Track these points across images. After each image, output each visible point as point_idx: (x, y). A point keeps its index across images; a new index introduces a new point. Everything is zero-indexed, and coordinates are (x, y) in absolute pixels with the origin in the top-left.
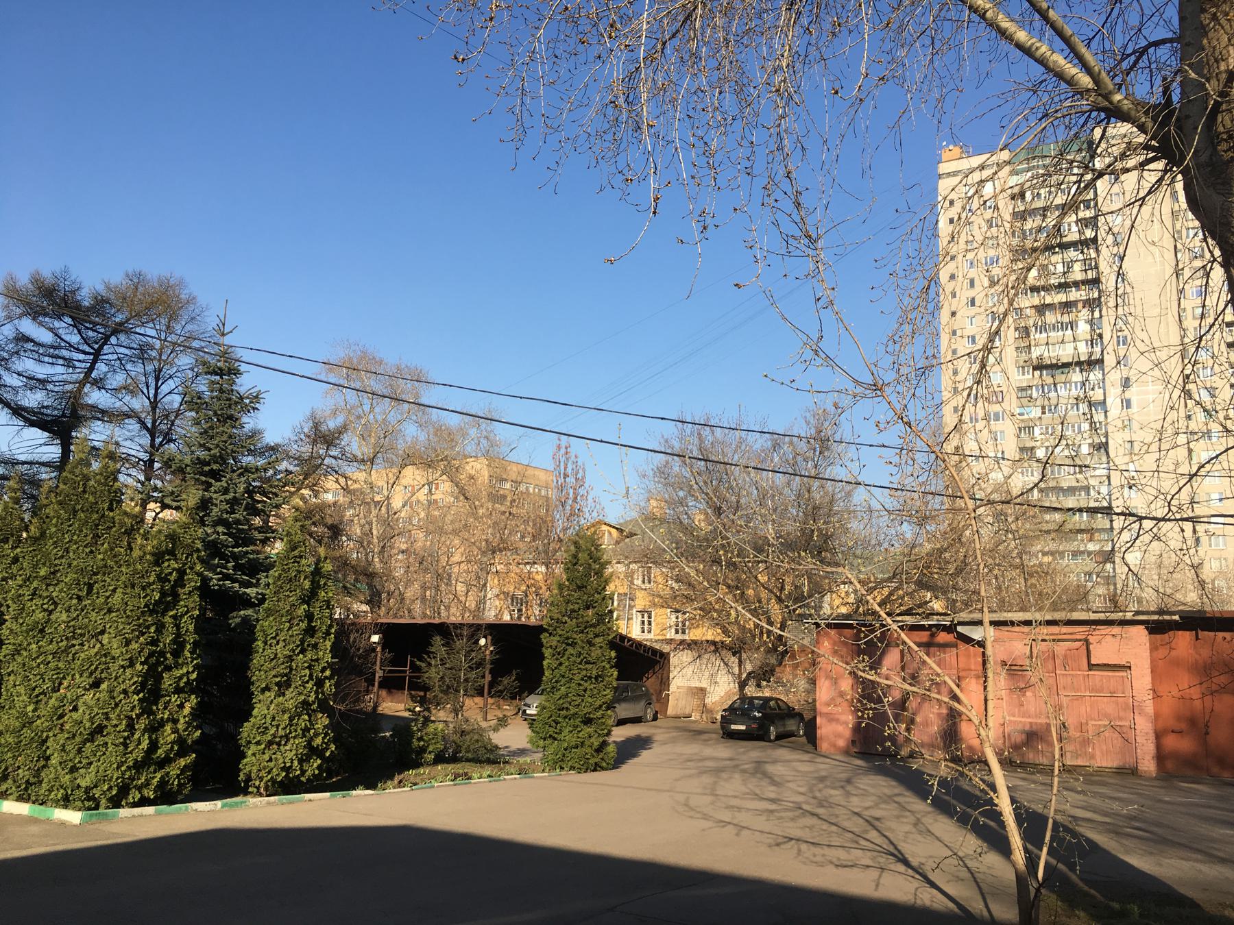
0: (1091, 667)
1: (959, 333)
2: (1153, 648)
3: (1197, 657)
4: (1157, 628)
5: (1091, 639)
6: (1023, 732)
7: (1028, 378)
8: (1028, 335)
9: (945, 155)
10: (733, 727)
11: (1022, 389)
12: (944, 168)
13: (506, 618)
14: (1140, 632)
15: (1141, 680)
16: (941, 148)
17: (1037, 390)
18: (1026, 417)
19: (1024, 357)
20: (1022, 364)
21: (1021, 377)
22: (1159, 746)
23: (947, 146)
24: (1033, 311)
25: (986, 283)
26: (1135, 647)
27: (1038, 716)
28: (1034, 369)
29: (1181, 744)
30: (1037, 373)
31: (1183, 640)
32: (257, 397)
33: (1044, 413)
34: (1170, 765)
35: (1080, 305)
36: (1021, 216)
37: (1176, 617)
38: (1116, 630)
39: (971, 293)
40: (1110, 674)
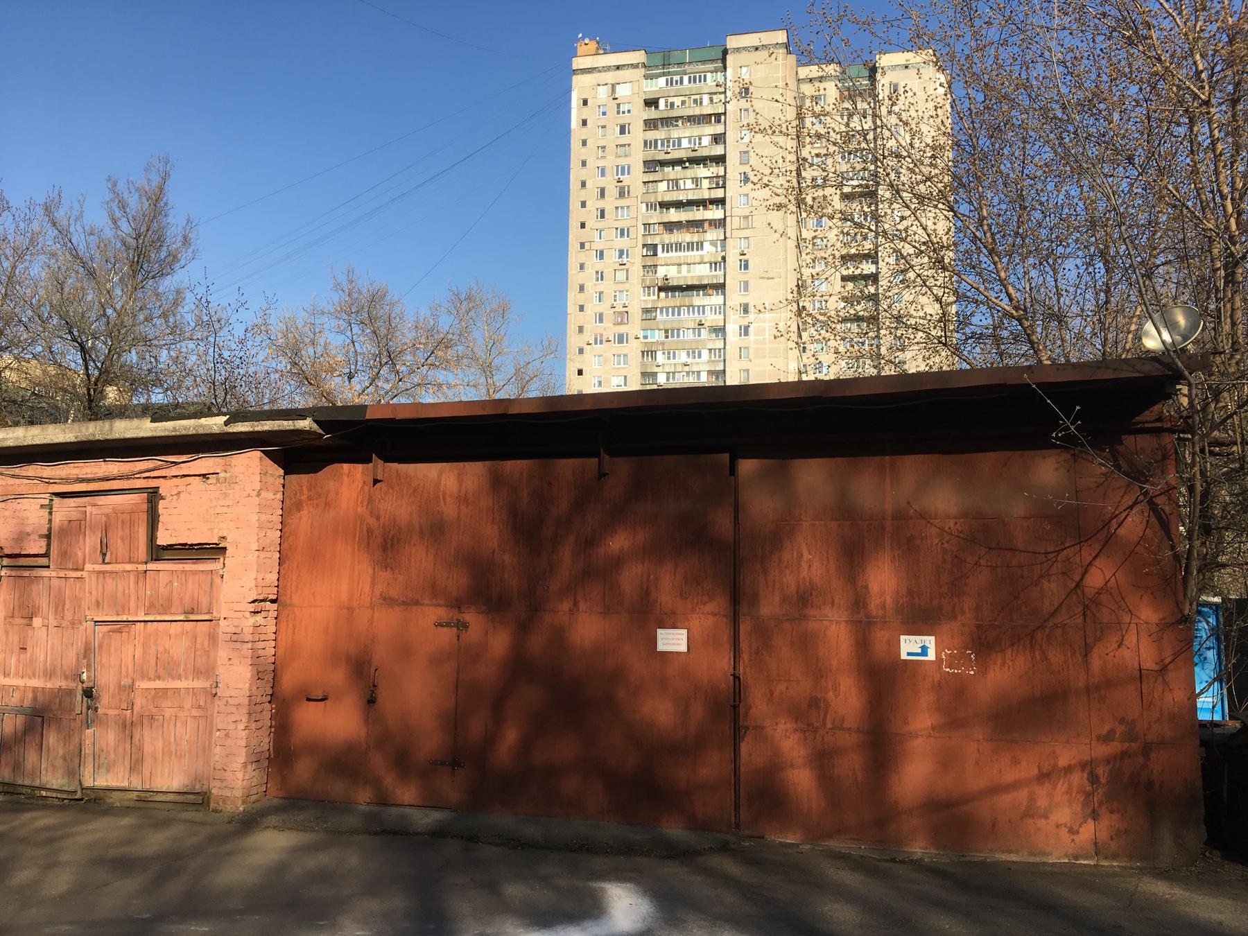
0: (157, 552)
1: (587, 246)
2: (289, 508)
3: (372, 521)
4: (295, 455)
5: (165, 487)
6: (19, 711)
7: (650, 299)
9: (581, 49)
10: (1204, 598)
12: (578, 63)
15: (243, 577)
16: (578, 40)
17: (661, 312)
19: (650, 276)
20: (648, 283)
21: (646, 298)
22: (282, 728)
23: (583, 38)
25: (616, 192)
27: (50, 674)
28: (660, 289)
29: (336, 722)
30: (663, 295)
31: (348, 483)
33: (667, 337)
34: (304, 770)
35: (706, 225)
36: (650, 124)
37: (305, 424)
38: (206, 463)
40: (189, 567)
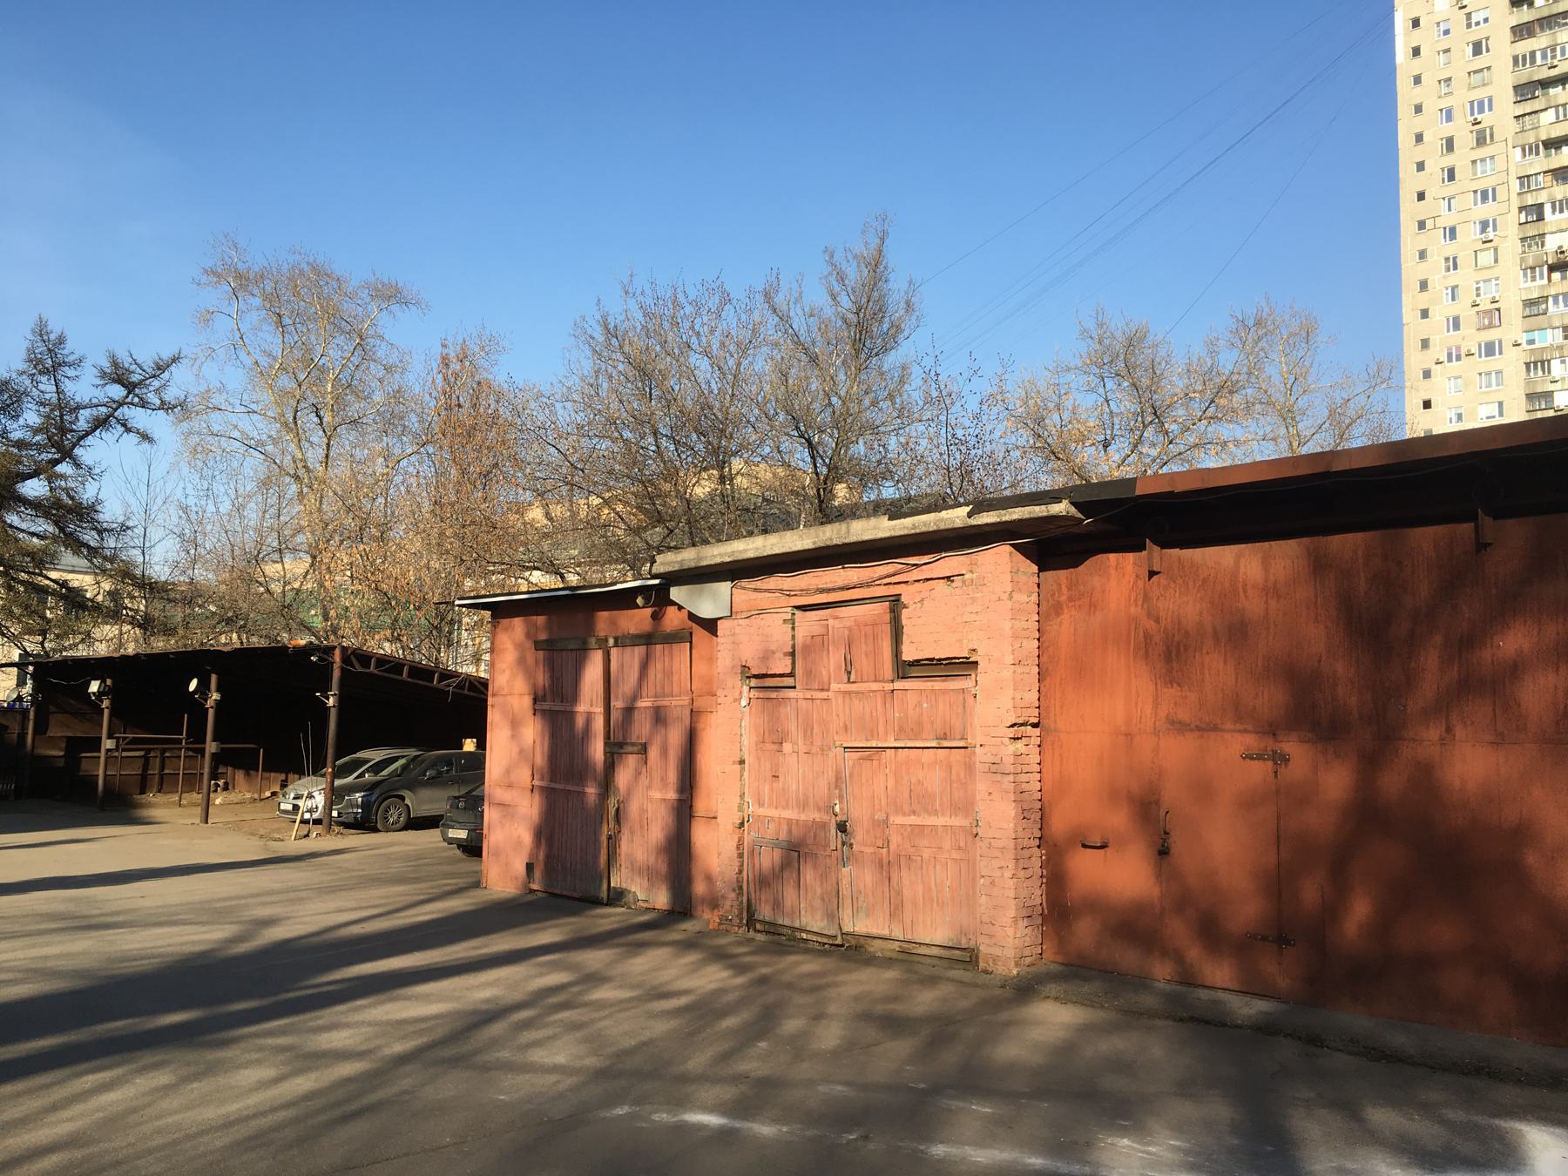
0: (904, 669)
1: (1429, 224)
2: (1047, 612)
3: (1150, 625)
5: (907, 594)
6: (775, 844)
8: (1541, 218)
11: (1529, 303)
13: (131, 649)
14: (1000, 565)
15: (999, 696)
18: (1537, 345)
20: (1531, 262)
21: (1530, 284)
22: (1055, 879)
24: (1549, 177)
26: (982, 605)
28: (1552, 269)
29: (1121, 875)
31: (1116, 576)
32: (41, 331)
34: (1085, 932)
37: (1061, 508)
38: (951, 563)
39: (1448, 161)
40: (938, 685)
